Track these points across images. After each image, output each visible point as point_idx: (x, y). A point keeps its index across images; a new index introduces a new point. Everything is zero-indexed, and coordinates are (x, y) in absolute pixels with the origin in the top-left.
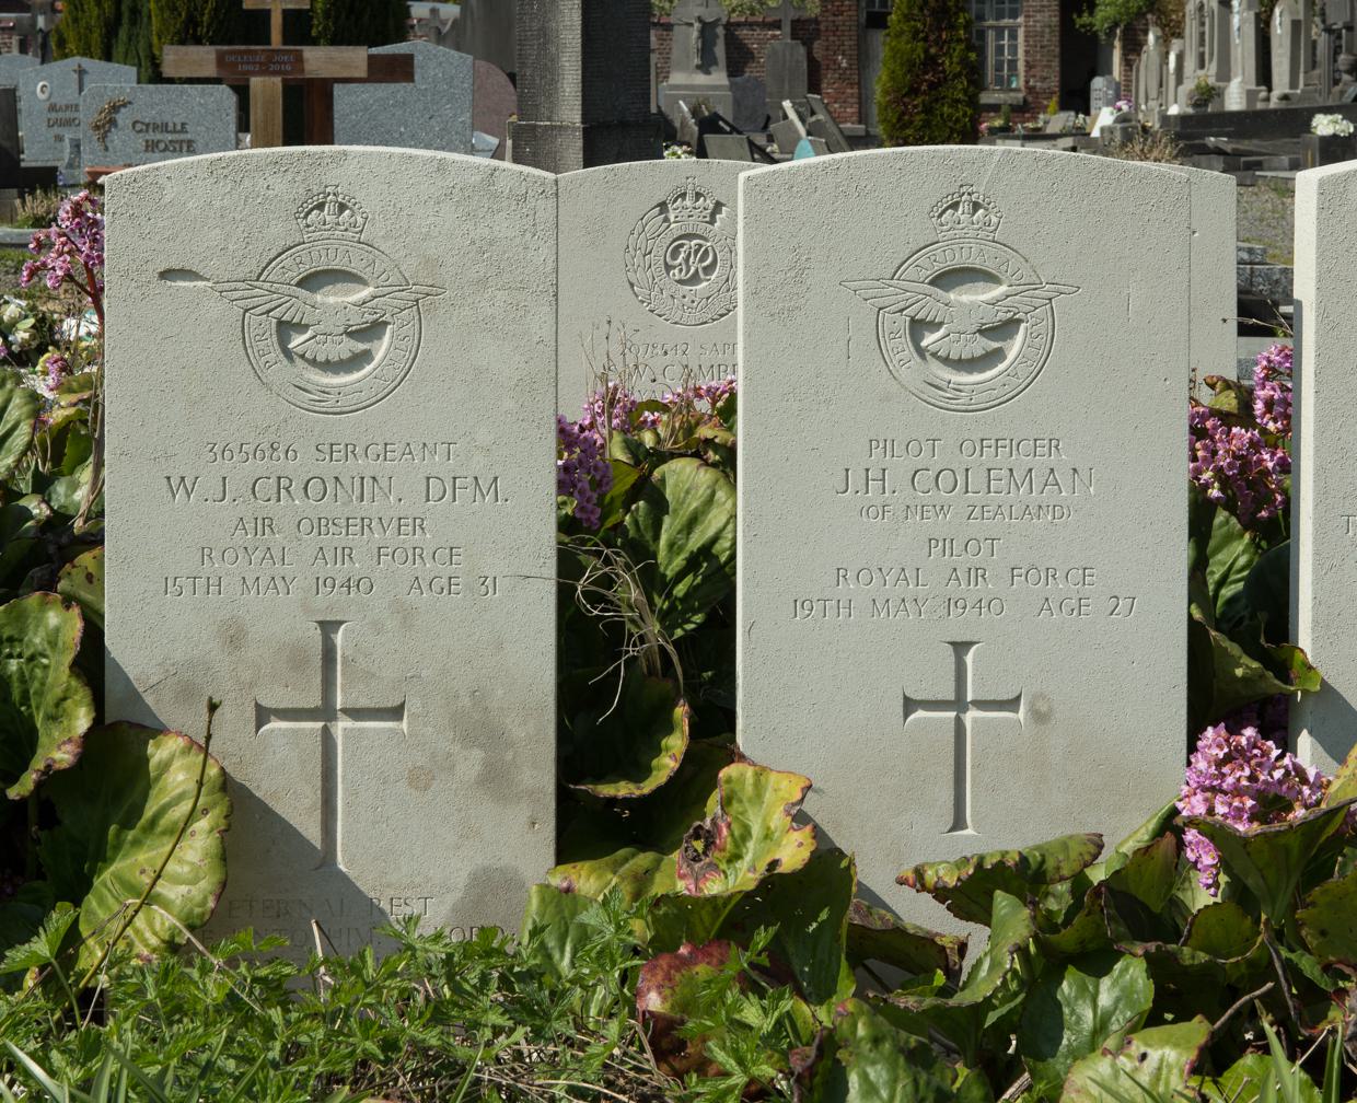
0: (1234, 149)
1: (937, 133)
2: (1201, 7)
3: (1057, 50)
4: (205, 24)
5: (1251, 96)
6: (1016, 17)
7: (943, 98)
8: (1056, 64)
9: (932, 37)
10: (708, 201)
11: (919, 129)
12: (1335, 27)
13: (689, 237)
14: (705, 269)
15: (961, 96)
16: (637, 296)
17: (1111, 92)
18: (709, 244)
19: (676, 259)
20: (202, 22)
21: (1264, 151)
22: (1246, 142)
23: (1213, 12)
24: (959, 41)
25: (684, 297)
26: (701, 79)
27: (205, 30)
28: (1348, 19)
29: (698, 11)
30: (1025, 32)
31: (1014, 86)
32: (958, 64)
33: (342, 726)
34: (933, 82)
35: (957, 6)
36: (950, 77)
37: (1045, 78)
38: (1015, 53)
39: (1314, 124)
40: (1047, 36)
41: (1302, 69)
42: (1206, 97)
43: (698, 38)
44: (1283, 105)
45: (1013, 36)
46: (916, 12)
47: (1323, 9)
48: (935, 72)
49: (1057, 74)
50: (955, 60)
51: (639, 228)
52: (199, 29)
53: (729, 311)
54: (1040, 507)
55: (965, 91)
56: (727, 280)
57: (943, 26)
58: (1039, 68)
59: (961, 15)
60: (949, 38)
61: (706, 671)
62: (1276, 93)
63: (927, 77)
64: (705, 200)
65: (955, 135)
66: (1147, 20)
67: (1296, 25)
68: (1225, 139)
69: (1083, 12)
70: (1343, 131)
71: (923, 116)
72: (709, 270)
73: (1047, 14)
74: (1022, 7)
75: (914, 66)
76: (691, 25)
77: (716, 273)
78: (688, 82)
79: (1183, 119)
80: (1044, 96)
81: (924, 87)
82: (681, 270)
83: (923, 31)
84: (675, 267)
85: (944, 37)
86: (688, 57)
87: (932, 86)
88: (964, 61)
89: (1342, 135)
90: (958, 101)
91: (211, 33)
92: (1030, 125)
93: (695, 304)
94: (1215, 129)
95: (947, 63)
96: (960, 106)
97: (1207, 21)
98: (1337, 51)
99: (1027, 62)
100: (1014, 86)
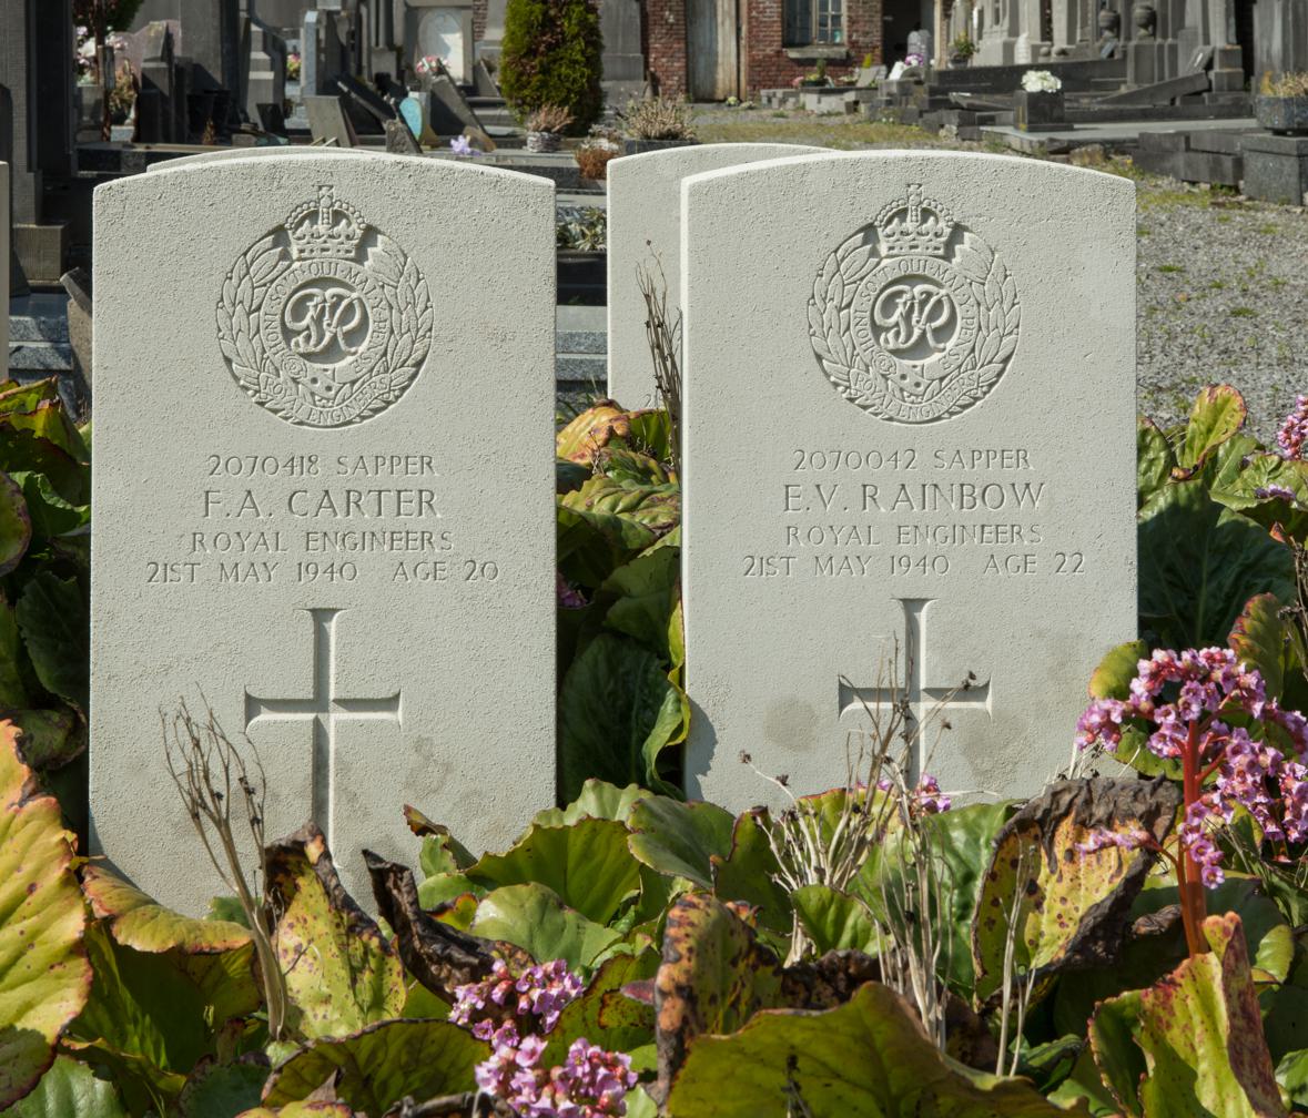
1: (553, 94)
5: (1035, 50)
13: (911, 279)
14: (936, 331)
15: (579, 57)
18: (354, 295)
19: (889, 317)
21: (1000, 106)
22: (984, 97)
25: (903, 377)
31: (838, 40)
33: (335, 719)
34: (550, 44)
38: (839, 9)
39: (1024, 81)
41: (1079, 25)
44: (1061, 59)
50: (573, 22)
51: (240, 269)
53: (389, 403)
55: (583, 52)
56: (385, 354)
61: (1101, 1081)
62: (1055, 49)
71: (540, 76)
77: (365, 344)
79: (943, 75)
81: (542, 48)
84: (887, 330)
87: (550, 47)
88: (583, 23)
90: (576, 62)
92: (845, 79)
93: (922, 388)
99: (849, 17)
100: (838, 40)
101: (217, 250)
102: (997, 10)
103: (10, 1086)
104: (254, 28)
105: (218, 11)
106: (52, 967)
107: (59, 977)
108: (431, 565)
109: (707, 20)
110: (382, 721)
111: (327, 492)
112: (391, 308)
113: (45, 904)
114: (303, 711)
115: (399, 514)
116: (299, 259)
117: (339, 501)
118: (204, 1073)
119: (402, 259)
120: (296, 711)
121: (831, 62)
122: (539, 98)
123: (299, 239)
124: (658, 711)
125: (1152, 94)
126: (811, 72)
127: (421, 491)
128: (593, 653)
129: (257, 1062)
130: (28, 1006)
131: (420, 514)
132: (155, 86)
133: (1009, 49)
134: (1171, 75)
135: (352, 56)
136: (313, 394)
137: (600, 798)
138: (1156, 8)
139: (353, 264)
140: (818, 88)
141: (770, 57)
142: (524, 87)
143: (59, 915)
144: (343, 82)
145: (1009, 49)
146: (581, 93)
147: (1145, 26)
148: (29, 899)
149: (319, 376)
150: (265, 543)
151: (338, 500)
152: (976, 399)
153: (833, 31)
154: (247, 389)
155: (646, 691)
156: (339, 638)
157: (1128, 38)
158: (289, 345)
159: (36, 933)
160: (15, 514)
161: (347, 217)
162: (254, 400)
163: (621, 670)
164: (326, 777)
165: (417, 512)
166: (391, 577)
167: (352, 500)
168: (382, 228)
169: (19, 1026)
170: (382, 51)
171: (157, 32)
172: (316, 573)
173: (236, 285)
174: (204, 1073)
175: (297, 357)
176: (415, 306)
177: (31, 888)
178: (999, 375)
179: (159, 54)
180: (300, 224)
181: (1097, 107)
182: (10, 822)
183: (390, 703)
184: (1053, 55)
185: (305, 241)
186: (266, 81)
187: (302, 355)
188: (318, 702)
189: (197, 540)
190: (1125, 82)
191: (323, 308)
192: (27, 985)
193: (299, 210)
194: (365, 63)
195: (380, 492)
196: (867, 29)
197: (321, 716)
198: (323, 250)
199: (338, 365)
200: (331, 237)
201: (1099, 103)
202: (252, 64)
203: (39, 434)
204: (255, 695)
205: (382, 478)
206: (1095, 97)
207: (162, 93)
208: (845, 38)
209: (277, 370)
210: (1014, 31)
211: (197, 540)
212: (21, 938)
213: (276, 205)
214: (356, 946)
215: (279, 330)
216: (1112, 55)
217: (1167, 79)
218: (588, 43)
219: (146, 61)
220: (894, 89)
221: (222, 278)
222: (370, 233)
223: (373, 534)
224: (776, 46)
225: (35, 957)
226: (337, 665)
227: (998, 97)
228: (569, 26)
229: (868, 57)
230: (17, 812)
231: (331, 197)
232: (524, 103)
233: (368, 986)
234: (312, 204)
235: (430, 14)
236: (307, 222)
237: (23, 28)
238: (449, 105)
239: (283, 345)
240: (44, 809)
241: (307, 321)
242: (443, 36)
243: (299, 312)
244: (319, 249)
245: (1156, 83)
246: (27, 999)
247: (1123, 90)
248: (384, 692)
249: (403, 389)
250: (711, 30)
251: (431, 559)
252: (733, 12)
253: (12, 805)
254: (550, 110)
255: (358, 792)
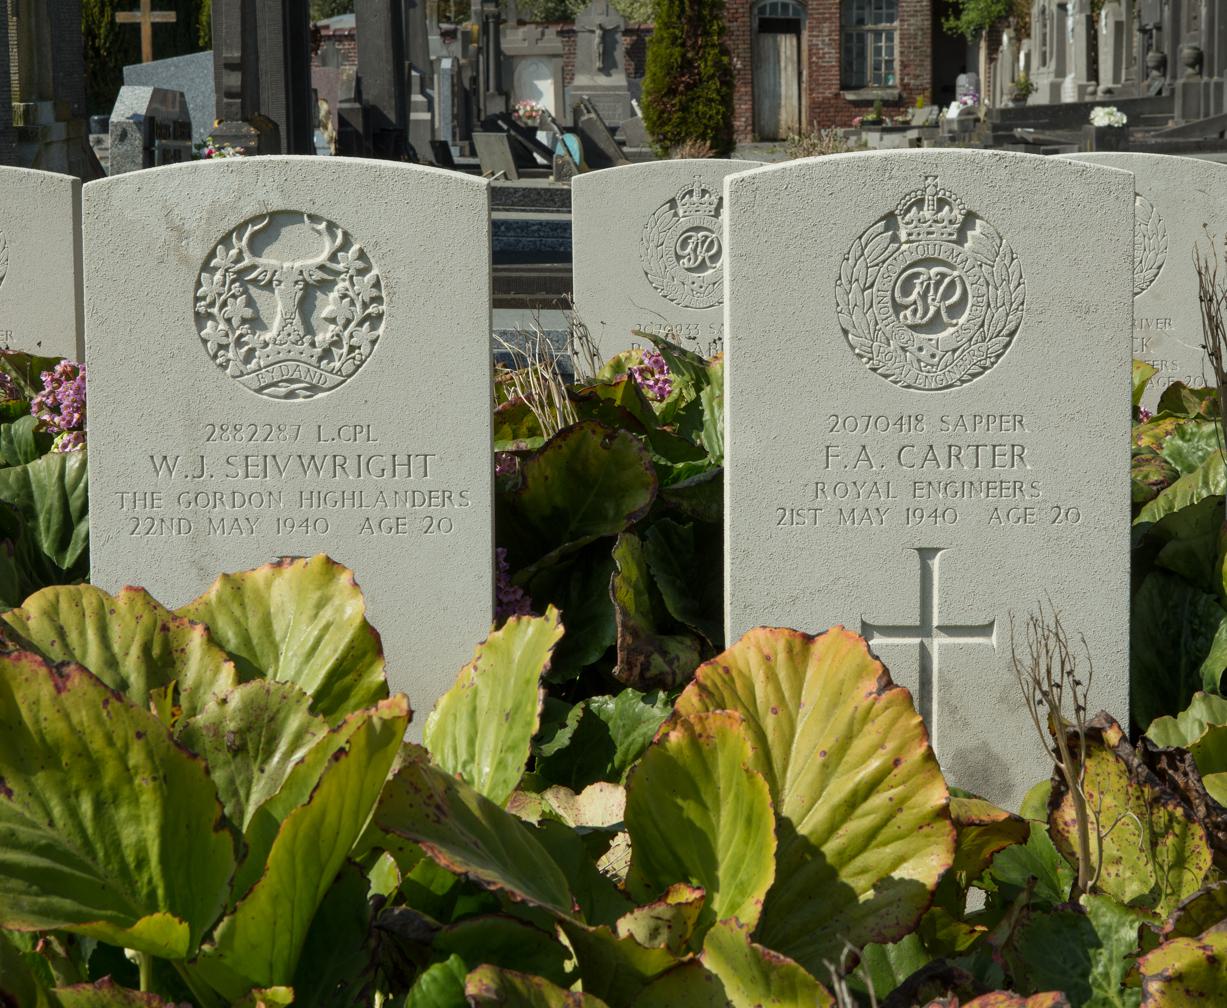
0: (1034, 139)
1: (692, 130)
2: (1043, 12)
3: (929, 51)
4: (102, 36)
5: (1081, 89)
6: (892, 21)
7: (699, 97)
8: (928, 63)
9: (689, 43)
10: (956, 212)
11: (677, 126)
12: (1148, 27)
14: (950, 309)
16: (652, 283)
17: (972, 88)
18: (956, 273)
20: (100, 34)
21: (1063, 140)
22: (1047, 133)
23: (1053, 15)
24: (713, 46)
26: (602, 80)
27: (102, 41)
28: (1158, 20)
29: (599, 20)
30: (901, 34)
31: (890, 83)
32: (712, 66)
33: (938, 643)
35: (711, 15)
36: (705, 78)
37: (918, 76)
39: (1092, 116)
40: (920, 38)
41: (1124, 66)
42: (1024, 92)
43: (600, 43)
45: (890, 39)
46: (674, 19)
47: (1139, 11)
48: (691, 74)
49: (929, 72)
50: (709, 63)
51: (855, 251)
52: (97, 41)
53: (985, 369)
54: (162, 520)
55: (718, 92)
56: (982, 325)
57: (699, 33)
58: (912, 67)
59: (715, 22)
60: (704, 44)
62: (1102, 88)
63: (683, 79)
64: (951, 210)
65: (709, 131)
66: (1009, 23)
67: (1118, 26)
68: (1032, 130)
69: (949, 16)
70: (1117, 122)
71: (680, 114)
72: (955, 310)
73: (919, 18)
74: (898, 12)
75: (672, 69)
76: (593, 32)
77: (965, 316)
78: (591, 83)
79: (1004, 112)
80: (917, 92)
81: (681, 88)
82: (689, 260)
83: (681, 38)
85: (700, 42)
86: (591, 61)
87: (689, 87)
88: (717, 64)
89: (1116, 125)
90: (711, 100)
91: (108, 45)
92: (900, 118)
93: (937, 359)
94: (1032, 121)
95: (702, 66)
96: (713, 104)
97: (1048, 22)
98: (1148, 48)
99: (902, 62)
100: (890, 83)
101: (836, 234)
102: (1044, 53)
103: (898, 924)
104: (414, 73)
105: (391, 57)
106: (921, 828)
107: (927, 836)
108: (1022, 510)
109: (772, 65)
110: (980, 644)
111: (931, 447)
112: (988, 284)
113: (910, 776)
114: (910, 637)
115: (994, 466)
116: (907, 242)
117: (941, 454)
118: (1029, 919)
119: (998, 241)
120: (904, 636)
121: (886, 103)
122: (679, 134)
123: (907, 223)
124: (1213, 638)
125: (1202, 127)
126: (868, 113)
127: (1013, 446)
128: (1149, 582)
129: (1074, 911)
130: (901, 860)
131: (1013, 466)
132: (350, 125)
133: (1055, 89)
134: (1216, 113)
135: (474, 99)
136: (919, 361)
137: (1210, 707)
138: (1202, 48)
139: (955, 245)
140: (876, 127)
141: (829, 99)
142: (663, 124)
143: (923, 785)
144: (503, 121)
145: (1055, 89)
146: (716, 129)
147: (1192, 66)
148: (895, 771)
149: (925, 345)
150: (878, 492)
151: (941, 453)
152: (1143, 290)
153: (887, 75)
154: (861, 356)
155: (1197, 621)
156: (942, 573)
157: (1174, 77)
158: (898, 318)
159: (904, 800)
160: (642, 469)
161: (949, 204)
162: (868, 366)
163: (1170, 603)
164: (930, 692)
165: (1010, 464)
166: (987, 521)
167: (953, 453)
168: (981, 214)
169: (897, 875)
170: (493, 95)
171: (348, 76)
172: (922, 517)
173: (852, 265)
174: (1029, 919)
175: (905, 328)
176: (1009, 282)
177: (897, 762)
178: (1156, 275)
179: (353, 96)
180: (908, 210)
181: (1153, 141)
182: (871, 707)
183: (985, 630)
184: (1100, 93)
185: (912, 225)
186: (424, 121)
187: (910, 327)
188: (923, 629)
189: (819, 488)
190: (1173, 118)
191: (928, 285)
192: (900, 842)
193: (907, 198)
194: (482, 107)
195: (978, 446)
196: (918, 72)
197: (925, 640)
198: (929, 233)
199: (941, 335)
200: (936, 221)
201: (1153, 136)
202: (412, 106)
203: (618, 403)
204: (870, 621)
205: (979, 434)
206: (1148, 132)
207: (357, 131)
208: (898, 81)
209: (888, 340)
210: (1061, 72)
211: (819, 488)
212: (890, 803)
213: (888, 193)
214: (1161, 815)
215: (889, 304)
216: (1160, 92)
217: (1212, 115)
218: (723, 83)
219: (341, 102)
220: (955, 127)
221: (840, 258)
222: (970, 217)
223: (972, 483)
224: (834, 89)
225: (905, 819)
226: (940, 597)
227: (1059, 132)
228: (705, 67)
229: (920, 98)
230: (876, 699)
231: (936, 186)
232: (665, 138)
233: (1171, 848)
234: (919, 193)
235: (523, 62)
236: (914, 209)
237: (282, 70)
238: (597, 140)
239: (893, 318)
240: (901, 697)
241: (914, 296)
242: (537, 82)
243: (907, 290)
244: (922, 233)
245: (1202, 119)
246: (900, 854)
247: (1171, 125)
248: (982, 621)
249: (998, 357)
250: (775, 74)
251: (1022, 505)
252: (795, 58)
253: (871, 694)
254: (694, 145)
255: (959, 705)
